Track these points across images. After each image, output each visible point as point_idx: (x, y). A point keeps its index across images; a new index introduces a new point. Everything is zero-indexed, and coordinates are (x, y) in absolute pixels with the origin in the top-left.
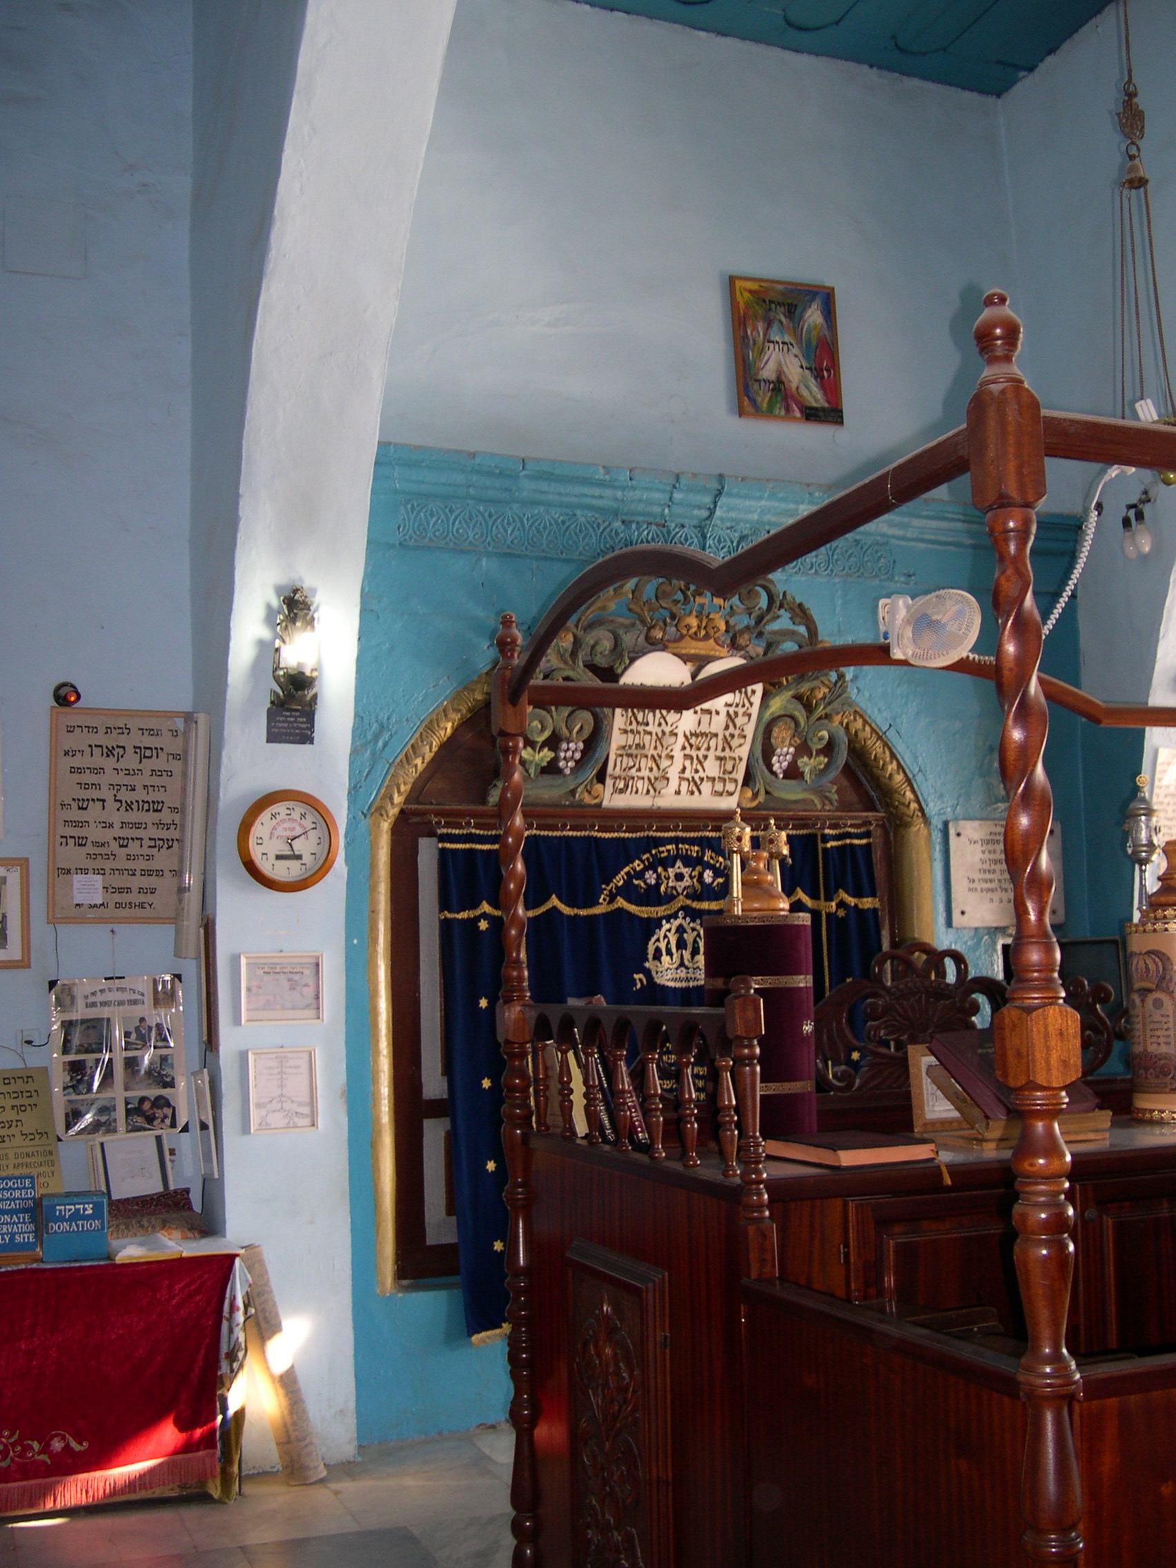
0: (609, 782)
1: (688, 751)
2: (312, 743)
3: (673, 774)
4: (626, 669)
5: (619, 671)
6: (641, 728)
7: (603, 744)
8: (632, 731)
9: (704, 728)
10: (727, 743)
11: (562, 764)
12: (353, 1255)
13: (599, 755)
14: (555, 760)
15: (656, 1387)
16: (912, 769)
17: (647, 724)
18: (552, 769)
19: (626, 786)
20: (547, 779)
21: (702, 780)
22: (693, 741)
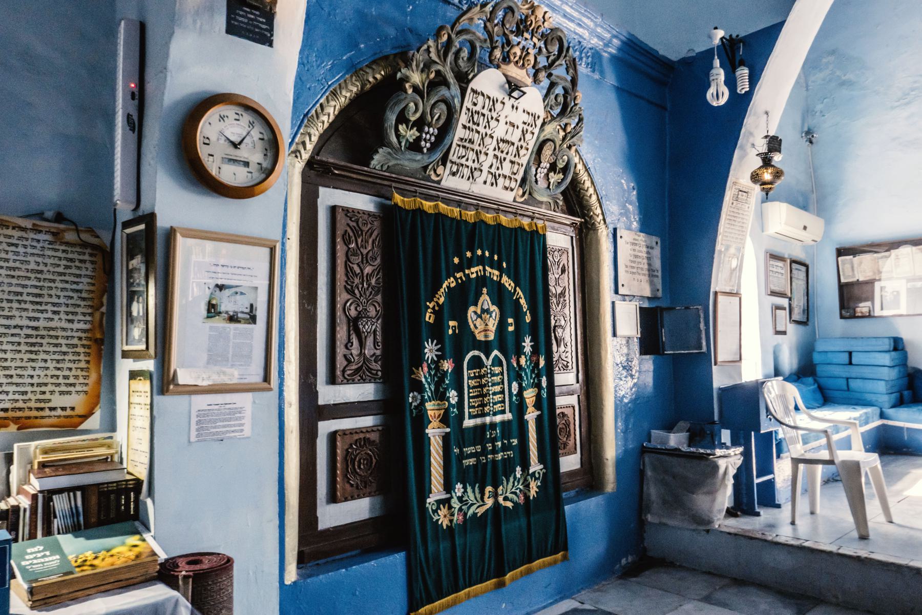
0: (449, 165)
1: (496, 152)
2: (271, 45)
3: (485, 168)
4: (474, 76)
5: (470, 77)
6: (475, 127)
7: (451, 135)
8: (469, 128)
9: (508, 138)
10: (518, 154)
11: (423, 143)
12: (280, 595)
13: (447, 142)
14: (419, 139)
15: (356, 538)
16: (602, 193)
17: (478, 125)
18: (415, 146)
19: (458, 170)
20: (410, 155)
21: (499, 175)
22: (501, 145)
